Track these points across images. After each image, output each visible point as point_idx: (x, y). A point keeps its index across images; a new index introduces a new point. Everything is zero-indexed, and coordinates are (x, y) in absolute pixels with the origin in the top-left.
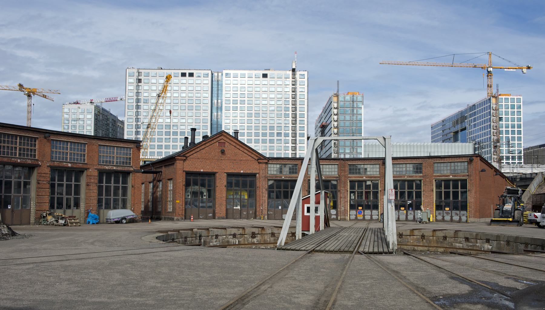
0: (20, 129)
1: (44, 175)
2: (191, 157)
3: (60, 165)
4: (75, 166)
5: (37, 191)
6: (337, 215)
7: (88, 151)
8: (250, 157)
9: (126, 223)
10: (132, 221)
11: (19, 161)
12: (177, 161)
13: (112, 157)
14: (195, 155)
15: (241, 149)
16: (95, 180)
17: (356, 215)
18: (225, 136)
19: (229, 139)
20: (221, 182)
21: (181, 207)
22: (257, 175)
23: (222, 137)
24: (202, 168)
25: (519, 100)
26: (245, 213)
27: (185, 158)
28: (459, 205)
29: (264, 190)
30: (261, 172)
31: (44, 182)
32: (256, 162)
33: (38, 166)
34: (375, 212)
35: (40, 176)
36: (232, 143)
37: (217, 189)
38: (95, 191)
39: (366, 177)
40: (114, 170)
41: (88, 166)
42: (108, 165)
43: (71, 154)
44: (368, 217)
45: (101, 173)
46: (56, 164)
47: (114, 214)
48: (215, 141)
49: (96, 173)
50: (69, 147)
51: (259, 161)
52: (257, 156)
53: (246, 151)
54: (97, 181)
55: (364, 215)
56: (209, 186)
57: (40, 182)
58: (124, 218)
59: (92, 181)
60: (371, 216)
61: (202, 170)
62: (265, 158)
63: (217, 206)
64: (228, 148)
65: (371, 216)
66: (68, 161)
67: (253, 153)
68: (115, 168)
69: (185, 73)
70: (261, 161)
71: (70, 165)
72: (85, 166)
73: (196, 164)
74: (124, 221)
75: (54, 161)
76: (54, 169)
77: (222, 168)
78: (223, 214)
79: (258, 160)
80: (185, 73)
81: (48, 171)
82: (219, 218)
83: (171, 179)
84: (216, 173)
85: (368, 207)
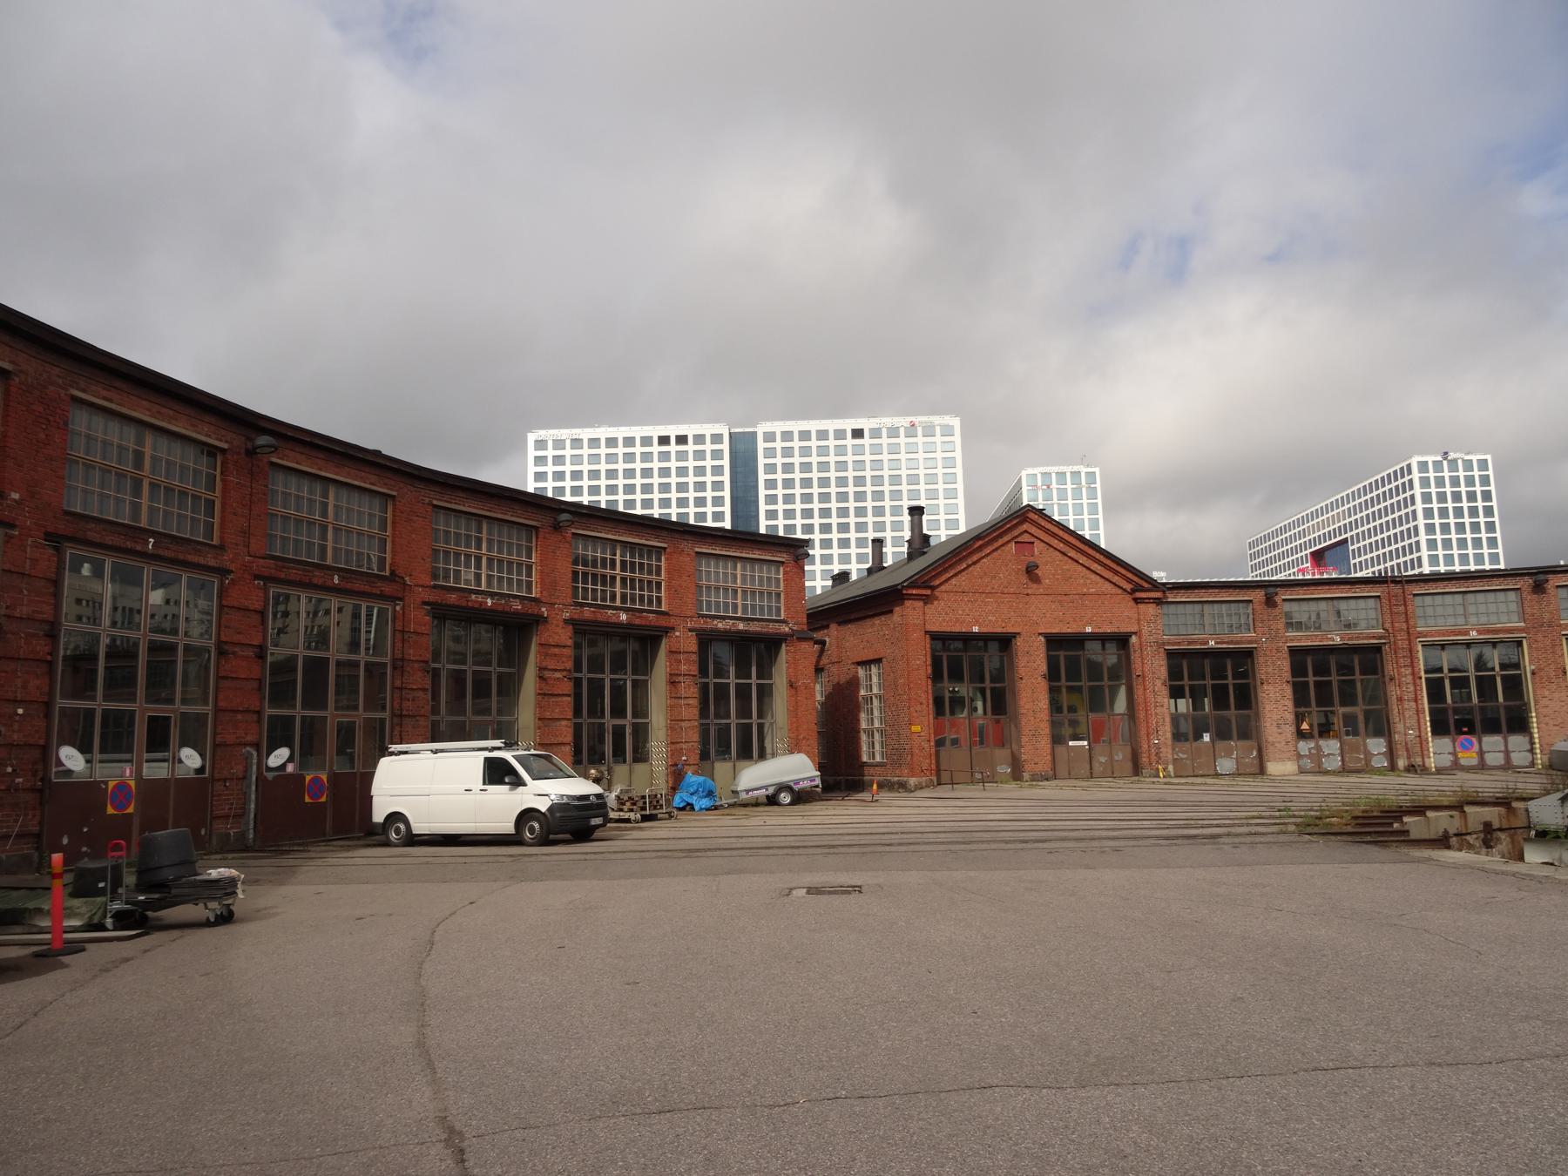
0: (485, 494)
1: (556, 651)
2: (943, 588)
3: (600, 618)
4: (637, 622)
5: (539, 705)
6: (1391, 754)
7: (668, 572)
8: (1108, 585)
9: (791, 804)
10: (801, 797)
11: (489, 602)
12: (908, 603)
13: (734, 595)
14: (953, 581)
15: (1083, 560)
16: (689, 666)
17: (1454, 754)
18: (1033, 523)
19: (1047, 531)
20: (1031, 664)
21: (926, 745)
22: (1134, 639)
23: (1025, 526)
24: (977, 623)
25: (1483, 465)
26: (1103, 760)
27: (928, 592)
28: (1452, 718)
29: (1159, 683)
30: (1145, 630)
31: (558, 675)
32: (1128, 597)
33: (539, 620)
34: (1517, 741)
35: (547, 655)
36: (1055, 542)
37: (1021, 685)
38: (691, 701)
39: (1479, 632)
40: (740, 632)
41: (672, 622)
42: (723, 618)
43: (623, 580)
44: (1495, 758)
45: (706, 639)
46: (587, 613)
47: (755, 776)
48: (1006, 539)
49: (692, 644)
50: (618, 558)
51: (1138, 595)
52: (1129, 581)
53: (1095, 567)
54: (695, 670)
55: (1481, 753)
56: (999, 676)
57: (547, 674)
58: (782, 787)
59: (684, 668)
60: (1507, 753)
61: (976, 629)
62: (1155, 585)
63: (1024, 739)
64: (1050, 562)
65: (1507, 753)
66: (618, 603)
67: (1116, 573)
68: (741, 626)
69: (703, 436)
70: (1144, 595)
71: (624, 617)
72: (663, 622)
73: (962, 609)
74: (785, 798)
75: (582, 605)
76: (581, 629)
77: (1033, 619)
78: (1044, 765)
79: (1133, 591)
80: (703, 436)
81: (565, 636)
82: (1034, 778)
83: (878, 661)
84: (1015, 635)
85: (1492, 727)
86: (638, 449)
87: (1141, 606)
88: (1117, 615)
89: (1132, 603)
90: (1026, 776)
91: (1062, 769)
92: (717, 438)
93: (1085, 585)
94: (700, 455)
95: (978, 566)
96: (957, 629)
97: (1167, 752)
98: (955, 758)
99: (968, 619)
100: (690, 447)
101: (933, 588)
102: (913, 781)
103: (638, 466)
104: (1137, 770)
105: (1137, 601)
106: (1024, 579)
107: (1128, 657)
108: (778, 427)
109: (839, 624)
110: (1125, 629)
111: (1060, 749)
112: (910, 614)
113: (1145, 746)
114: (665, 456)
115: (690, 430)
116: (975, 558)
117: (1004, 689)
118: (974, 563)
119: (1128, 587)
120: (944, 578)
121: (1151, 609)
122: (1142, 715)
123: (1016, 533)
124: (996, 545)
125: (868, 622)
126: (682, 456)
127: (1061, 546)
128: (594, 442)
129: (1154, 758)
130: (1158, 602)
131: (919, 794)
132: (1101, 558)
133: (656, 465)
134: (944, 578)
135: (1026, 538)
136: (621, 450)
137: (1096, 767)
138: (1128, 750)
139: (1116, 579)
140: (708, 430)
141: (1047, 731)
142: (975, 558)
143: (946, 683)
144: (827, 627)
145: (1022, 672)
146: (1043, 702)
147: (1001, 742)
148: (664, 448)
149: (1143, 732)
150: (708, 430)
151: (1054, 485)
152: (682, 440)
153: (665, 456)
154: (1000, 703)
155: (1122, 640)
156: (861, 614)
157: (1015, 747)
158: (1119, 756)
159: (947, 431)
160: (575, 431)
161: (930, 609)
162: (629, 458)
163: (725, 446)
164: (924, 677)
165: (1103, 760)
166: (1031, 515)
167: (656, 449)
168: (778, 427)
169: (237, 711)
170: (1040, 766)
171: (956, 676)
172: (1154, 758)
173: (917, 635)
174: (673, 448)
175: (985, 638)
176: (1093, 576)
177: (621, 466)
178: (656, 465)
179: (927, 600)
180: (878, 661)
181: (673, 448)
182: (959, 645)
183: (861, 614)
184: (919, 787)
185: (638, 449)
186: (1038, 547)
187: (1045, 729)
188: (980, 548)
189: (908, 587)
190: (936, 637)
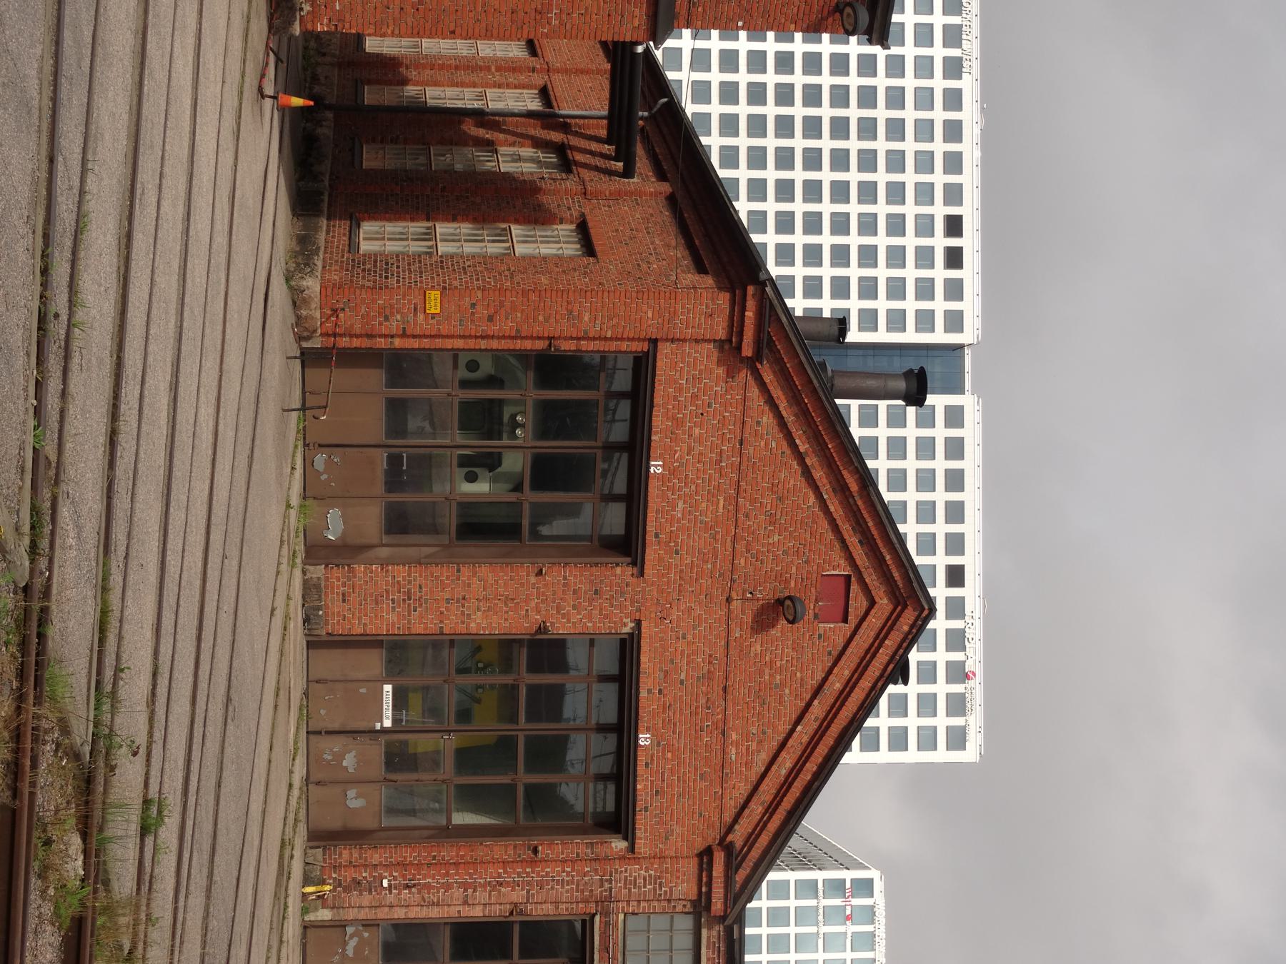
2: (754, 392)
8: (743, 789)
12: (723, 299)
14: (768, 419)
15: (803, 733)
22: (619, 845)
23: (884, 603)
24: (671, 471)
26: (349, 761)
27: (747, 351)
29: (518, 895)
30: (637, 871)
32: (713, 836)
36: (845, 670)
37: (525, 573)
51: (719, 858)
52: (751, 840)
63: (401, 572)
67: (771, 809)
73: (702, 427)
77: (677, 617)
78: (344, 617)
79: (728, 848)
82: (310, 588)
84: (638, 562)
86: (939, 178)
87: (692, 866)
88: (678, 796)
89: (700, 845)
90: (318, 571)
91: (331, 663)
92: (955, 321)
93: (747, 736)
94: (925, 290)
95: (800, 482)
96: (659, 421)
97: (359, 907)
98: (362, 402)
99: (680, 450)
100: (940, 273)
101: (752, 364)
102: (312, 285)
103: (910, 178)
104: (321, 837)
105: (705, 855)
106: (764, 594)
107: (583, 831)
108: (971, 433)
109: (671, 200)
110: (644, 824)
111: (374, 661)
112: (703, 306)
113: (376, 857)
114: (925, 226)
115: (970, 273)
116: (819, 474)
117: (507, 955)
118: (807, 473)
119: (737, 837)
120: (777, 393)
121: (685, 888)
122: (448, 853)
123: (871, 578)
124: (846, 528)
125: (673, 238)
126: (924, 256)
127: (836, 684)
128: (954, 100)
129: (349, 875)
130: (700, 907)
131: (279, 292)
132: (806, 776)
133: (910, 209)
134: (777, 393)
135: (858, 603)
136: (939, 147)
137: (336, 744)
138: (369, 823)
139: (756, 809)
140: (971, 306)
141: (418, 628)
142: (819, 474)
143: (536, 394)
144: (662, 176)
145: (555, 576)
146: (484, 622)
147: (399, 523)
148: (939, 226)
149: (408, 854)
150: (971, 306)
151: (851, 928)
152: (954, 258)
153: (925, 226)
154: (484, 529)
155: (618, 821)
156: (694, 228)
157: (384, 552)
158: (354, 800)
159: (957, 739)
160: (976, 65)
161: (706, 356)
162: (924, 161)
163: (939, 336)
164: (552, 329)
165: (349, 761)
166: (909, 616)
167: (940, 211)
168: (971, 433)
169: (493, 337)
170: (337, 607)
171: (553, 420)
172: (349, 875)
173: (649, 320)
174: (940, 242)
175: (634, 497)
176: (764, 757)
177: (910, 146)
178: (910, 209)
179: (729, 348)
180: (589, 248)
181: (940, 242)
182: (619, 432)
183: (694, 228)
184: (297, 299)
185: (939, 178)
186: (837, 632)
187: (422, 623)
188: (841, 488)
189: (762, 298)
190: (643, 366)
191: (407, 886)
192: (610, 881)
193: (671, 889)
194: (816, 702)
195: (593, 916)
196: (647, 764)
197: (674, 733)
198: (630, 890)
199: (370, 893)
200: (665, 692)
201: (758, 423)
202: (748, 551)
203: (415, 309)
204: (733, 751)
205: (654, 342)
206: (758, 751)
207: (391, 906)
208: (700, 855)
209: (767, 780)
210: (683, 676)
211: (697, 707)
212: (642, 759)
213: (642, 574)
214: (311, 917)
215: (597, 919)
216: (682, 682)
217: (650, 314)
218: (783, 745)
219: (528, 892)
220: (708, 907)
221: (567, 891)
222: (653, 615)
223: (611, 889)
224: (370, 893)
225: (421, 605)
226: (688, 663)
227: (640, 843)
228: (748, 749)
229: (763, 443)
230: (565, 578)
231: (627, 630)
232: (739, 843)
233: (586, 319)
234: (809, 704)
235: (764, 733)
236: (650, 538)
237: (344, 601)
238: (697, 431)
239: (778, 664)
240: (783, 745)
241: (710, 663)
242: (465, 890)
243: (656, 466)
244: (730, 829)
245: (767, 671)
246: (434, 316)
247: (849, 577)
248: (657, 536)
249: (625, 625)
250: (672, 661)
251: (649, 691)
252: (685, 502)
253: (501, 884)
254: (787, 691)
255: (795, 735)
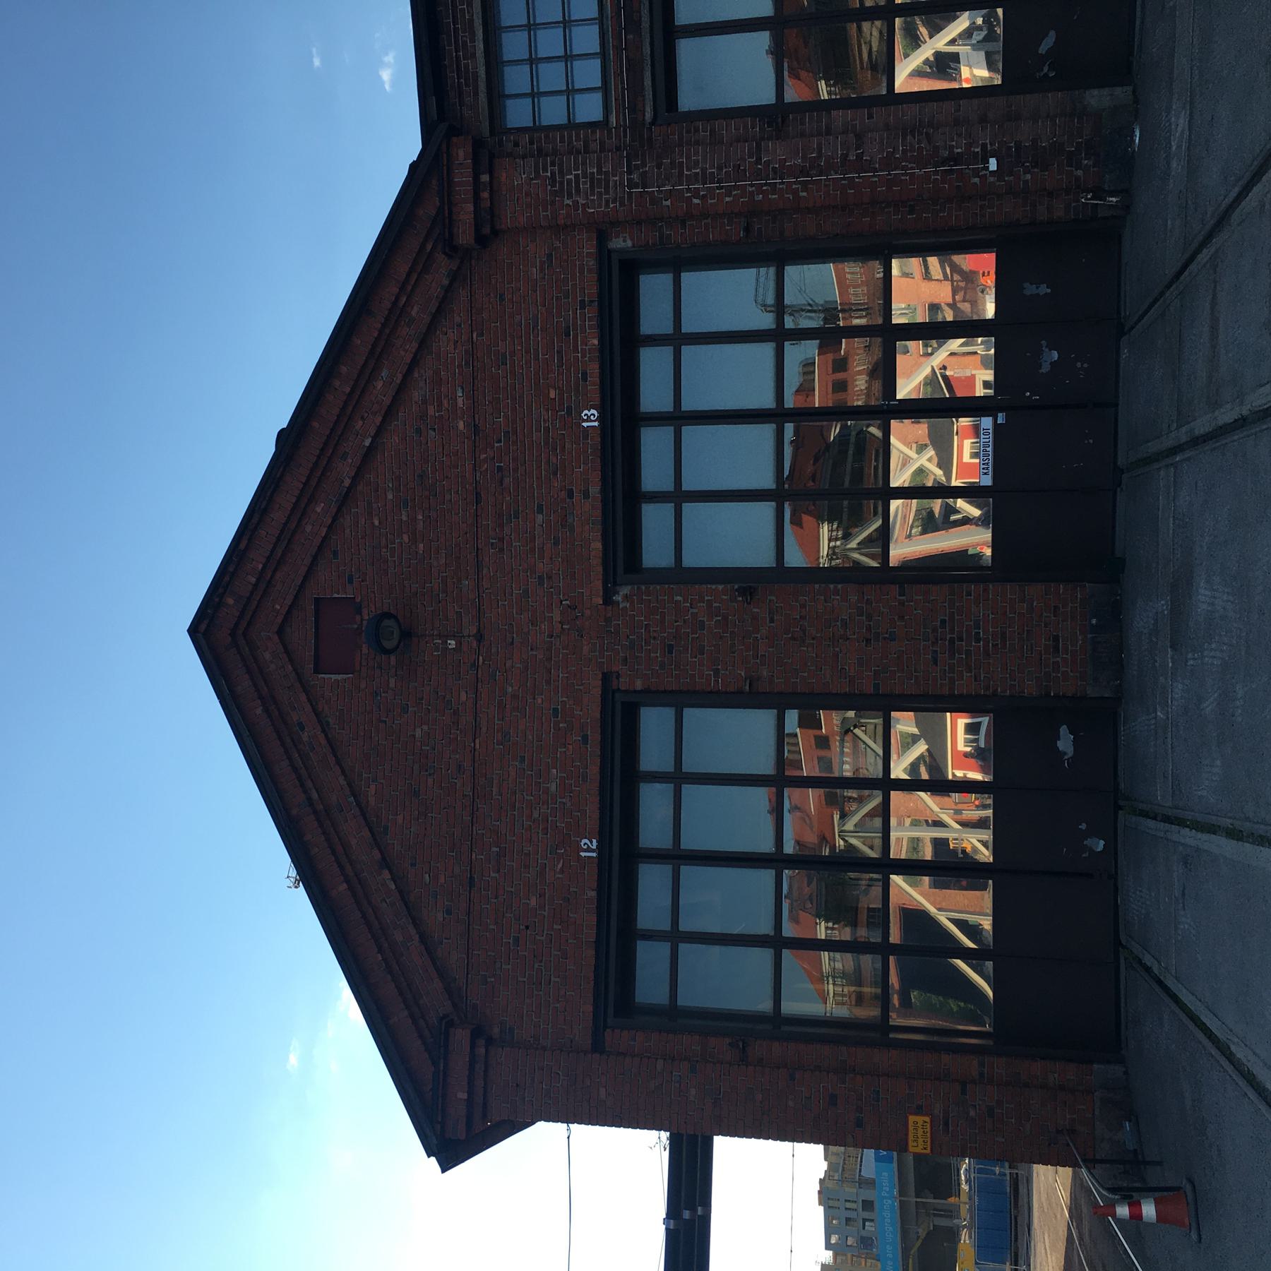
22: (621, 243)
27: (461, 1037)
51: (465, 236)
79: (451, 248)
191: (956, 159)
192: (632, 185)
193: (537, 176)
194: (347, 482)
195: (653, 123)
196: (585, 379)
197: (547, 429)
198: (600, 172)
199: (1018, 146)
200: (563, 494)
201: (449, 912)
202: (456, 713)
203: (946, 1124)
204: (460, 401)
205: (598, 1046)
206: (425, 402)
207: (983, 120)
208: (495, 233)
209: (408, 358)
210: (540, 518)
211: (516, 470)
212: (593, 387)
213: (606, 678)
214: (1122, 93)
215: (649, 116)
216: (540, 511)
217: (602, 1091)
218: (389, 414)
219: (759, 160)
220: (478, 144)
221: (696, 163)
222: (588, 612)
223: (629, 172)
224: (1018, 146)
225: (935, 630)
226: (533, 539)
227: (588, 247)
228: (440, 405)
229: (442, 880)
230: (717, 672)
231: (625, 590)
232: (440, 257)
233: (693, 1091)
234: (355, 479)
235: (419, 431)
236: (594, 736)
237: (1056, 639)
238: (533, 902)
239: (406, 538)
240: (389, 414)
241: (501, 540)
242: (859, 157)
243: (589, 850)
244: (454, 277)
245: (420, 526)
246: (919, 1111)
247: (317, 671)
248: (585, 739)
249: (626, 596)
250: (556, 543)
251: (586, 495)
252: (547, 791)
253: (803, 172)
254: (390, 496)
255: (372, 431)
